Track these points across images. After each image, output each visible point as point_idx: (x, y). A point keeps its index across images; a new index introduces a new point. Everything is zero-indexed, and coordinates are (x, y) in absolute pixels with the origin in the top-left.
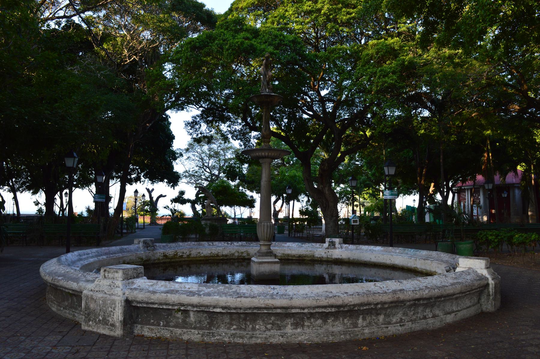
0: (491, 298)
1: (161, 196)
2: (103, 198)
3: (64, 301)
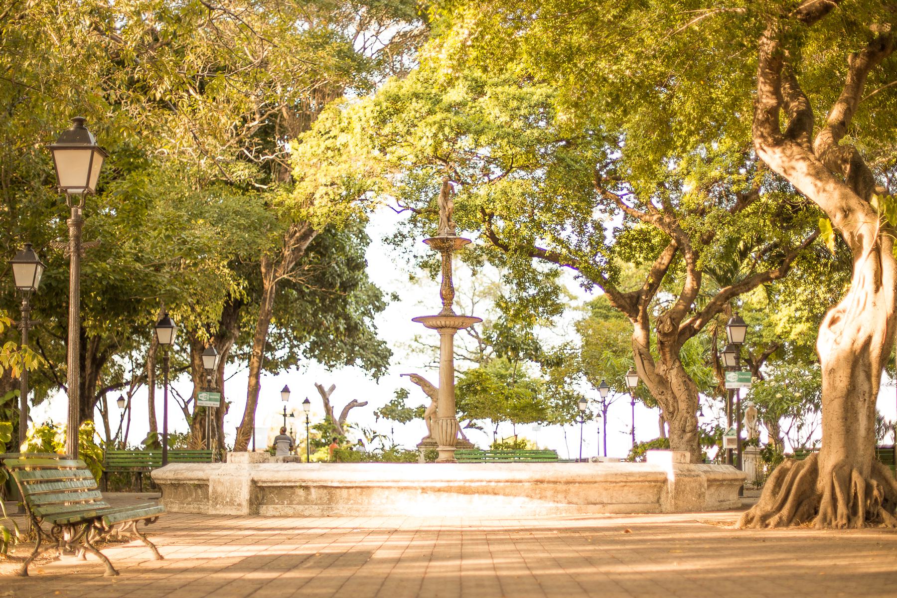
0: (670, 495)
1: (354, 404)
2: (216, 400)
3: (187, 498)
